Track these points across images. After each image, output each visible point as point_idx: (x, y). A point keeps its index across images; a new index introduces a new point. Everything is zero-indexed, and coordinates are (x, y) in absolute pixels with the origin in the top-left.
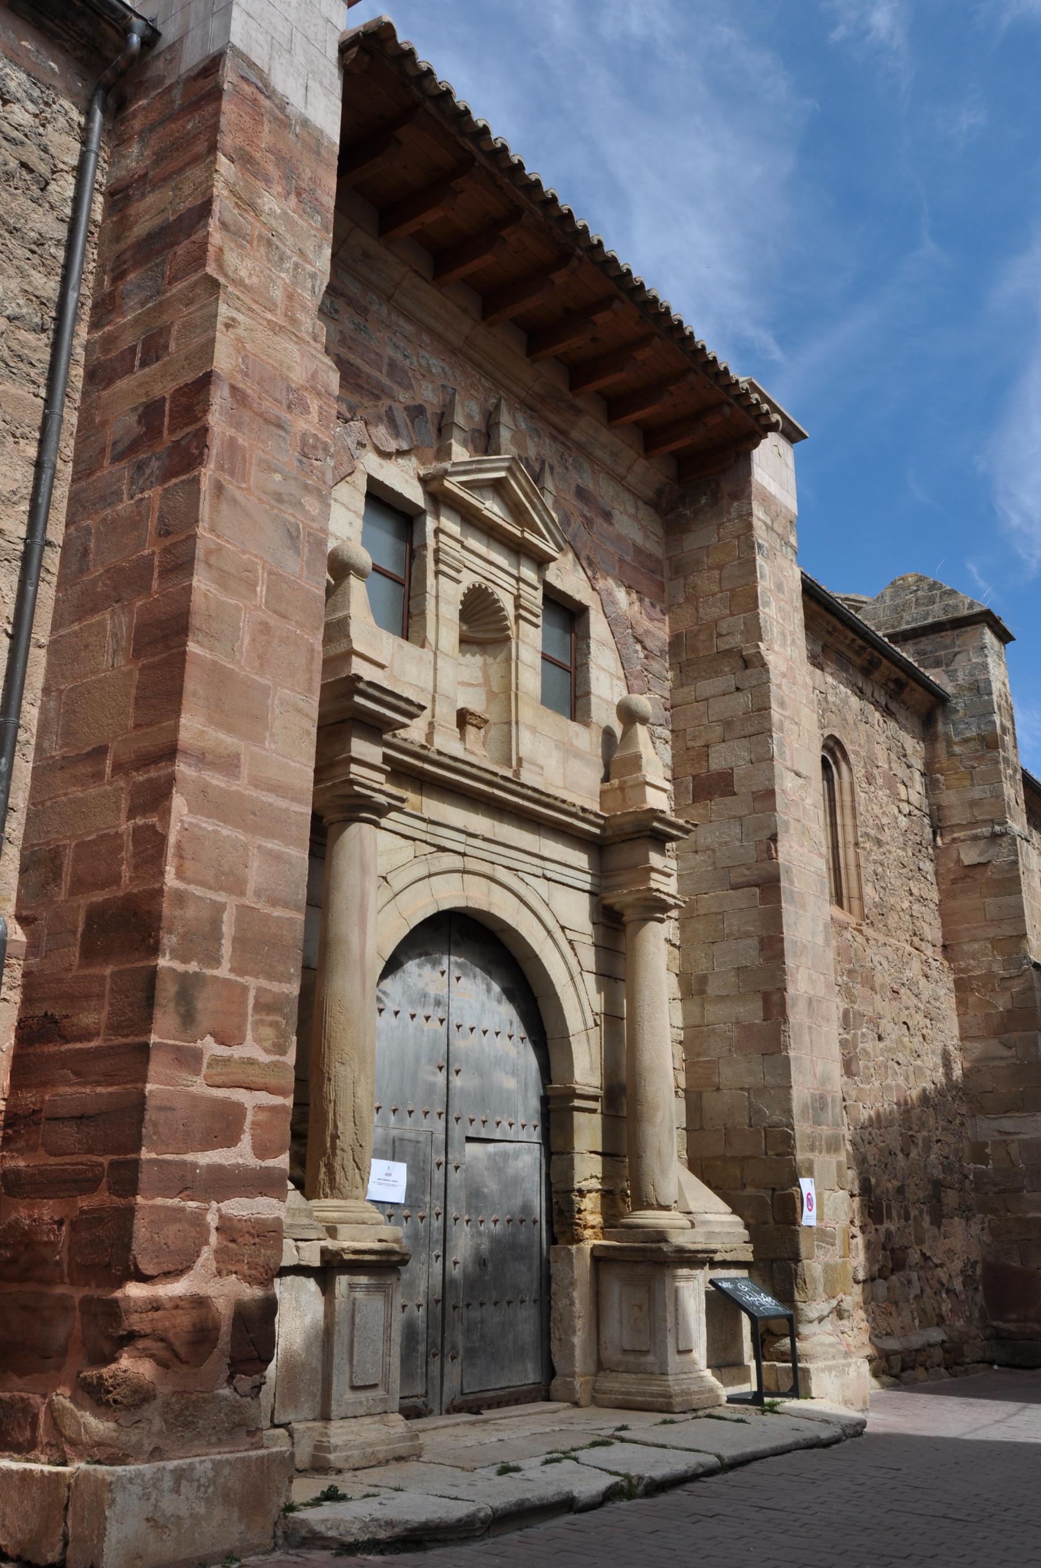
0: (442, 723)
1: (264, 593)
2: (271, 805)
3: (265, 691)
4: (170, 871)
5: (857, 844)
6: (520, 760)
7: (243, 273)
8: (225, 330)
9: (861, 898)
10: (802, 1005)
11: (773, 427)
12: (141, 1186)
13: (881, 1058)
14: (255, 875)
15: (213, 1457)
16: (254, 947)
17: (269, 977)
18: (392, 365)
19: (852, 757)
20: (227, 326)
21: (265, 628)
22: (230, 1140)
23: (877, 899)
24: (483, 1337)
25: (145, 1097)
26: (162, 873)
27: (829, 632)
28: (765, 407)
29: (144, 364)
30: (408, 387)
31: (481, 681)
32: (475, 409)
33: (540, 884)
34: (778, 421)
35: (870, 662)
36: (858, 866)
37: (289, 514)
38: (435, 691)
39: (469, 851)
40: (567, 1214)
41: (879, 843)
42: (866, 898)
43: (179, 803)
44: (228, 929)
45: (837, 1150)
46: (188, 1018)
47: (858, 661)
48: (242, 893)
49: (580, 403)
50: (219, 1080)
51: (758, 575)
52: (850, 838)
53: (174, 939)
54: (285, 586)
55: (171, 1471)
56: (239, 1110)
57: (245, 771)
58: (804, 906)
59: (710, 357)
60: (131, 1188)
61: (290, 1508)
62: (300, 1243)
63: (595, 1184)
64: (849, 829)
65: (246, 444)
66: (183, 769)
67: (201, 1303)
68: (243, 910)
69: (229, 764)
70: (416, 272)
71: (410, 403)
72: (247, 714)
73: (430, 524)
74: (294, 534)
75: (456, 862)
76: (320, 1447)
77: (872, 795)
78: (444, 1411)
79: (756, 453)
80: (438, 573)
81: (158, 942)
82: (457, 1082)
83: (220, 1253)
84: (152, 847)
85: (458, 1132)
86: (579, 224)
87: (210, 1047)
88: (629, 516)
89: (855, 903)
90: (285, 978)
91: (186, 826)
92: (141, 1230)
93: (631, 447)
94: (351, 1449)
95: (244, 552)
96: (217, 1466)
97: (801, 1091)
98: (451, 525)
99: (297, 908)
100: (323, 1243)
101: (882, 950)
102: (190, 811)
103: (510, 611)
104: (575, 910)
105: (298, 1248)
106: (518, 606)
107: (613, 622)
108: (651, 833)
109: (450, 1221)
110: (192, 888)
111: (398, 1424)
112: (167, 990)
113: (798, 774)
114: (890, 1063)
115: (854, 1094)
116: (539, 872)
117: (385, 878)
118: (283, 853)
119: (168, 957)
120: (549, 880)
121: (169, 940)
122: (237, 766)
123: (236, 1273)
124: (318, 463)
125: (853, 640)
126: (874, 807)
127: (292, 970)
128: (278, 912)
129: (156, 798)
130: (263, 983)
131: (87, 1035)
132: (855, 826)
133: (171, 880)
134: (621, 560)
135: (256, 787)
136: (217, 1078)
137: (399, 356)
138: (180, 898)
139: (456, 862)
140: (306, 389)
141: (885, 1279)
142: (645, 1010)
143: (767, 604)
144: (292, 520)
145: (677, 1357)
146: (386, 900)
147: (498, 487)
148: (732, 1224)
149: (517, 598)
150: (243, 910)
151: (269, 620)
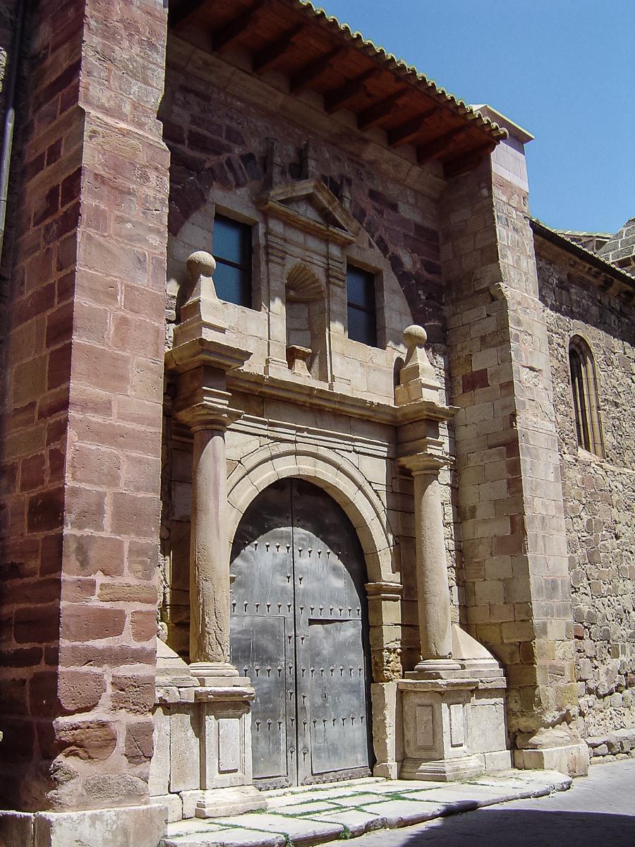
0: (275, 359)
1: (123, 300)
2: (133, 430)
3: (126, 360)
4: (68, 475)
5: (598, 408)
6: (333, 377)
7: (104, 100)
8: (89, 140)
9: (602, 444)
10: (537, 523)
11: (503, 137)
12: (60, 660)
13: (618, 550)
14: (125, 473)
15: (115, 809)
16: (127, 517)
17: (138, 534)
18: (229, 130)
19: (593, 349)
20: (91, 137)
21: (123, 321)
22: (117, 631)
23: (615, 443)
24: (326, 740)
25: (60, 610)
26: (63, 477)
27: (571, 265)
28: (494, 124)
29: (48, 164)
30: (242, 143)
31: (307, 326)
32: (291, 151)
33: (353, 457)
34: (505, 133)
35: (605, 282)
36: (600, 422)
37: (139, 248)
38: (269, 339)
39: (298, 439)
40: (380, 664)
41: (616, 405)
42: (606, 444)
43: (71, 433)
44: (108, 509)
45: (565, 614)
46: (84, 562)
47: (595, 282)
48: (117, 485)
49: (367, 135)
50: (107, 597)
51: (498, 237)
52: (594, 403)
53: (73, 516)
54: (137, 293)
55: (89, 816)
56: (121, 613)
57: (115, 410)
58: (537, 457)
59: (449, 98)
60: (55, 662)
61: (166, 836)
62: (180, 689)
63: (398, 645)
64: (593, 398)
65: (107, 209)
66: (73, 413)
67: (103, 725)
68: (118, 497)
69: (105, 408)
70: (240, 69)
71: (244, 153)
72: (115, 375)
73: (261, 229)
74: (142, 259)
75: (291, 447)
76: (201, 805)
77: (609, 373)
78: (299, 785)
79: (492, 154)
80: (267, 262)
81: (63, 519)
82: (301, 586)
83: (115, 698)
84: (58, 459)
85: (303, 618)
86: (342, 26)
87: (100, 578)
88: (411, 205)
89: (599, 448)
90: (150, 534)
91: (77, 448)
92: (61, 684)
93: (407, 159)
94: (219, 805)
95: (108, 275)
96: (117, 815)
97: (537, 577)
98: (277, 227)
99: (154, 491)
100: (196, 689)
101: (619, 478)
102: (79, 439)
103: (323, 279)
104: (375, 470)
105: (179, 692)
106: (328, 276)
107: (403, 277)
108: (431, 419)
109: (300, 672)
110: (83, 485)
111: (252, 791)
112: (70, 548)
113: (532, 369)
114: (625, 553)
115: (596, 575)
116: (351, 448)
117: (240, 462)
118: (143, 458)
119: (69, 527)
120: (358, 453)
121: (69, 517)
122: (110, 408)
123: (125, 708)
124: (158, 212)
125: (590, 269)
126: (612, 380)
127: (153, 529)
128: (141, 495)
129: (60, 431)
130: (133, 537)
131: (33, 574)
132: (597, 395)
133: (69, 483)
134: (405, 236)
135: (123, 419)
136: (106, 596)
137: (234, 125)
138: (75, 492)
139: (291, 447)
140: (147, 166)
141: (621, 692)
142: (427, 533)
143: (505, 256)
144: (140, 250)
145: (452, 749)
146: (241, 476)
147: (310, 199)
148: (492, 665)
149: (327, 270)
150: (118, 497)
151: (127, 316)
